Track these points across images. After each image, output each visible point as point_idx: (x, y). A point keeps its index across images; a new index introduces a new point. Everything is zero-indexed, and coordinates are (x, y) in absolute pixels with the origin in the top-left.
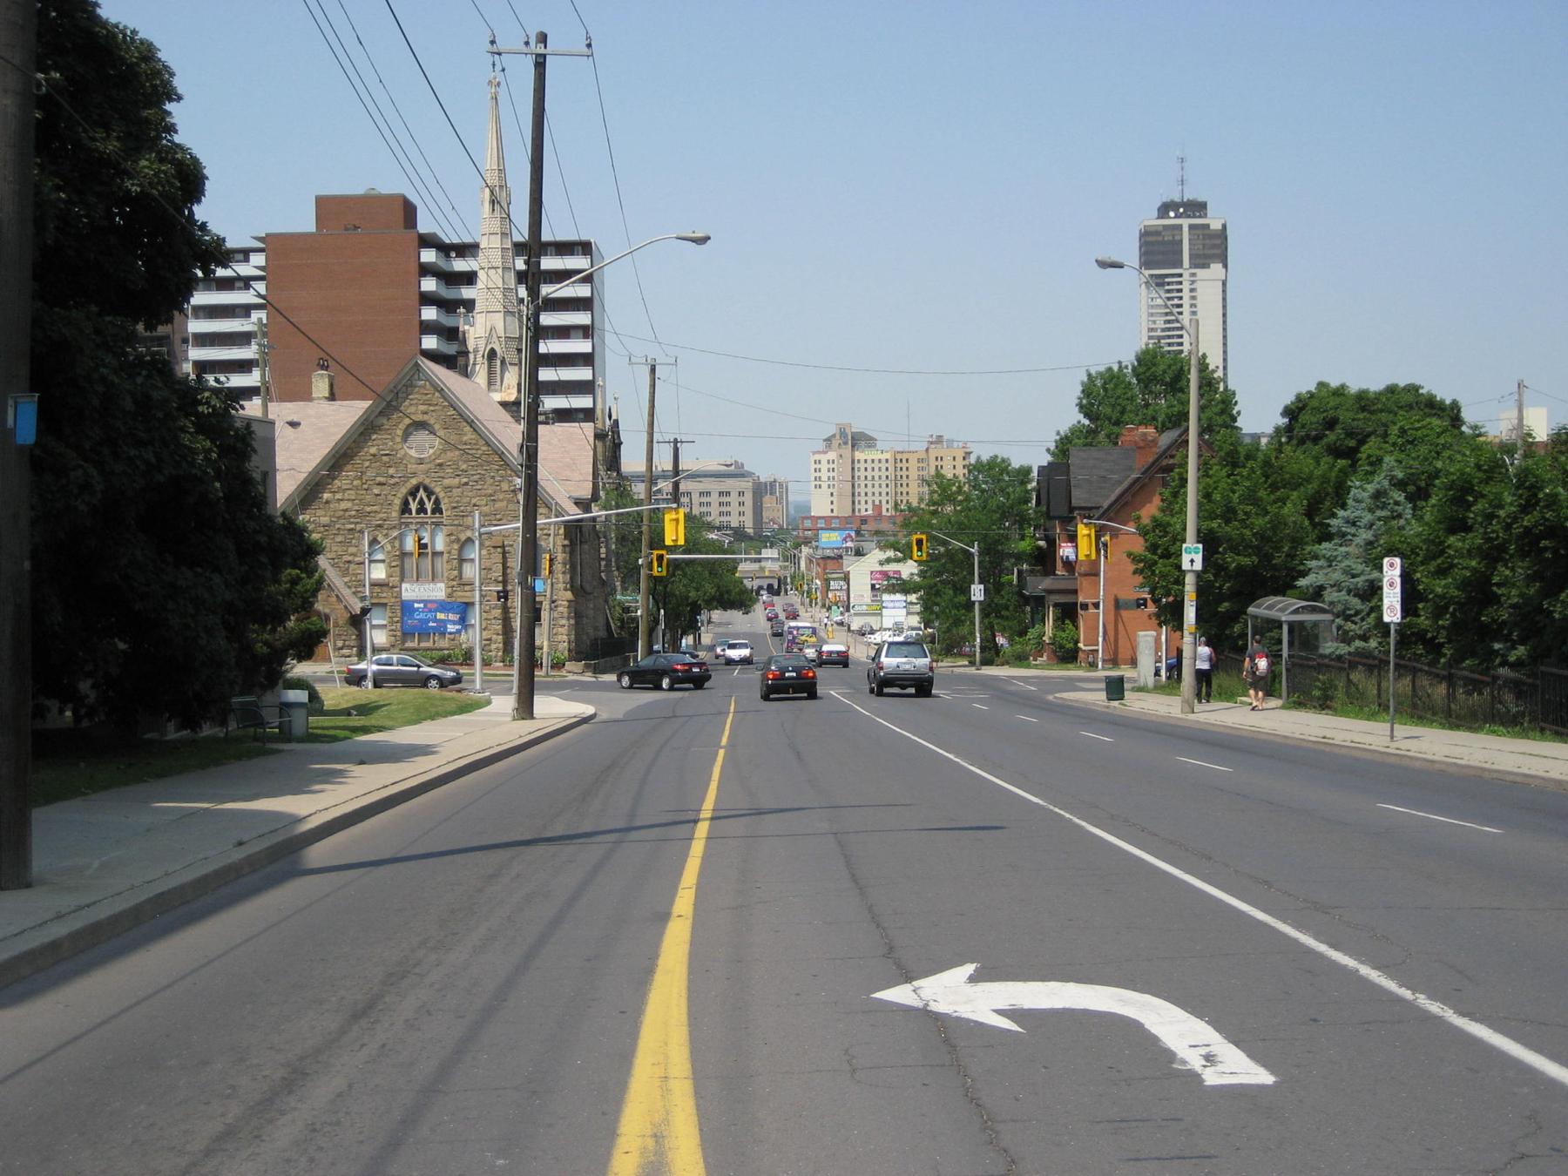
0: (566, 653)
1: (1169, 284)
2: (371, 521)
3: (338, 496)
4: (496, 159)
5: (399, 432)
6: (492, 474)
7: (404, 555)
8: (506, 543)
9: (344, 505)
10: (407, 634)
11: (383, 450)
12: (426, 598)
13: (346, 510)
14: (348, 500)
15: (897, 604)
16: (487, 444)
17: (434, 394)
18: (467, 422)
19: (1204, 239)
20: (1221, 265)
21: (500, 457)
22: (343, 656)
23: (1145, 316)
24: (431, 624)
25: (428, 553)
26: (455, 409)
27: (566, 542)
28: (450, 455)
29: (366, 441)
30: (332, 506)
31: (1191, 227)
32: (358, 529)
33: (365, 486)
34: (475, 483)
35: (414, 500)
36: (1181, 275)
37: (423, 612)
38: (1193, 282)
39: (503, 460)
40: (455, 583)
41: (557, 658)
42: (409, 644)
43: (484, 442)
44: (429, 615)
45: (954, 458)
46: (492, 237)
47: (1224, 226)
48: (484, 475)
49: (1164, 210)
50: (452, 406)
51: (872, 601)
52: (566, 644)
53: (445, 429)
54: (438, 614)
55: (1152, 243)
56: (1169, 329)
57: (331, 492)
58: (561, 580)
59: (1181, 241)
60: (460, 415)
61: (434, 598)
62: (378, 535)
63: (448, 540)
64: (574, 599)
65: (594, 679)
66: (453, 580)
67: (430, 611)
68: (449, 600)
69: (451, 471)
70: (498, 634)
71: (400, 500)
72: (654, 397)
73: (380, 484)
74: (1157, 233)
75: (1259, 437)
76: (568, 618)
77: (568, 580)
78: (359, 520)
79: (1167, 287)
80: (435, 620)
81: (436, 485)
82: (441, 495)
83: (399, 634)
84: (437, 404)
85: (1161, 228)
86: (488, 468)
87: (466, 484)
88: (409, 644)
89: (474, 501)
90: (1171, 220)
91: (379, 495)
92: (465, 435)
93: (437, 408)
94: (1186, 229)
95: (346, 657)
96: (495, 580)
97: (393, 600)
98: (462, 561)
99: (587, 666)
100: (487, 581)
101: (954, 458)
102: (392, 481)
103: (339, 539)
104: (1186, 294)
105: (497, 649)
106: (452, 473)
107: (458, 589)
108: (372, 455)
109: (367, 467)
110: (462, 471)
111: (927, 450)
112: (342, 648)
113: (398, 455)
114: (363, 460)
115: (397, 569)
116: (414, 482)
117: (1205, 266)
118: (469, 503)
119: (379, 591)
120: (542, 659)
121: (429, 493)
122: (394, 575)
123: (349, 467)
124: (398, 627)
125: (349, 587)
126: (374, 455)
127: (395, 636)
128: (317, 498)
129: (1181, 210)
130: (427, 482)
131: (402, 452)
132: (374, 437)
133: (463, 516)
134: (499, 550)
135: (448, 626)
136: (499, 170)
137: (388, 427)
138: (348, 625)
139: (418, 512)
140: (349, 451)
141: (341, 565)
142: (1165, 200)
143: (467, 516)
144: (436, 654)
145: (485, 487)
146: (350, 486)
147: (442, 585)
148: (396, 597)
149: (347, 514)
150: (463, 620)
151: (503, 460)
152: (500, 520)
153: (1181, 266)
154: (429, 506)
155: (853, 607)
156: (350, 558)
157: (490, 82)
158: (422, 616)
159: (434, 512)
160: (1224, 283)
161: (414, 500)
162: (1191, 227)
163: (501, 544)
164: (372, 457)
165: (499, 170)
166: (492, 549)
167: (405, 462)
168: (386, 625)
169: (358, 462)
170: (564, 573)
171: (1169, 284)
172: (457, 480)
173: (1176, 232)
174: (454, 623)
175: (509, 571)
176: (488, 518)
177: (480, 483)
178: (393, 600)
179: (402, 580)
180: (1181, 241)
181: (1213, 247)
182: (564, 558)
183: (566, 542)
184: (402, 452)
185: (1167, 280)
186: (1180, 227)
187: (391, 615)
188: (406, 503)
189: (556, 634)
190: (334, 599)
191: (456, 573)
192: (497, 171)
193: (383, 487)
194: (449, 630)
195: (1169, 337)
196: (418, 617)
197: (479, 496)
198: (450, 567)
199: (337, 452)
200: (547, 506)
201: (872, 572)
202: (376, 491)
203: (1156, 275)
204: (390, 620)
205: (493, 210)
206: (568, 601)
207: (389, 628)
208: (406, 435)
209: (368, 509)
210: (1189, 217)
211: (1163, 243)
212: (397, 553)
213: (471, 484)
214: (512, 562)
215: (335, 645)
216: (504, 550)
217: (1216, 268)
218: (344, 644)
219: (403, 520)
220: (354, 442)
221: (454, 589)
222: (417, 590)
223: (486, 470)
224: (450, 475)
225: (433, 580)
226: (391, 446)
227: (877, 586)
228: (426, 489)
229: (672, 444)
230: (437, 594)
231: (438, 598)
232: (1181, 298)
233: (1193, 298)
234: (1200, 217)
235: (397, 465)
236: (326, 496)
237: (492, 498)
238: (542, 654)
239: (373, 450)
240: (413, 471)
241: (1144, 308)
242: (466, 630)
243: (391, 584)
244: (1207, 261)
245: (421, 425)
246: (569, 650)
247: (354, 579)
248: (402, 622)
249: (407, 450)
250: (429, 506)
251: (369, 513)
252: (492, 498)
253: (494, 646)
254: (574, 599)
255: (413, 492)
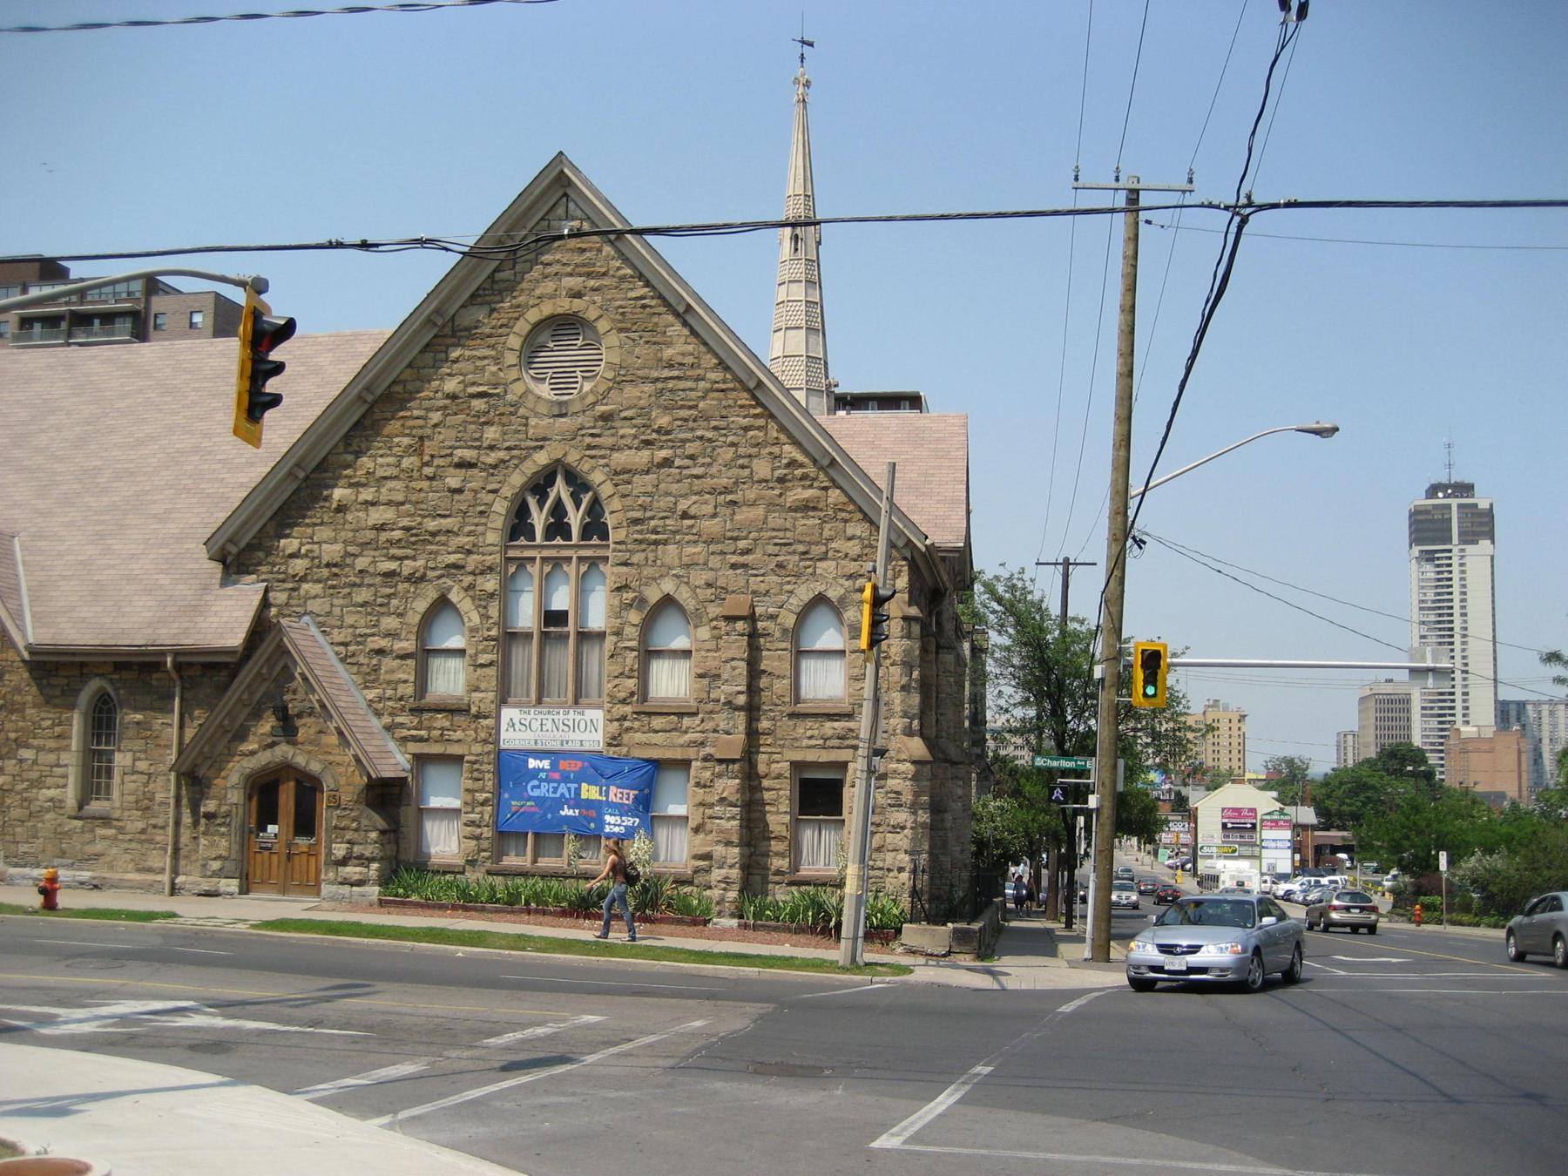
0: (905, 902)
1: (1438, 559)
2: (437, 553)
3: (367, 494)
4: (802, 180)
5: (514, 342)
6: (731, 439)
7: (510, 638)
8: (758, 610)
9: (377, 516)
10: (505, 837)
11: (474, 384)
12: (557, 747)
13: (381, 528)
14: (389, 503)
15: (1279, 844)
16: (722, 365)
17: (599, 250)
18: (677, 315)
19: (1472, 517)
20: (1489, 542)
21: (754, 397)
22: (345, 882)
23: (1415, 589)
24: (567, 812)
25: (567, 636)
26: (648, 284)
27: (914, 611)
28: (630, 392)
29: (436, 366)
30: (349, 517)
31: (1460, 506)
32: (406, 571)
33: (428, 471)
34: (687, 462)
35: (541, 504)
36: (1450, 551)
37: (548, 780)
38: (1462, 557)
39: (759, 404)
40: (628, 709)
41: (882, 911)
42: (511, 861)
43: (715, 361)
44: (563, 789)
45: (1230, 721)
46: (794, 286)
47: (1491, 505)
48: (710, 440)
49: (1433, 491)
50: (641, 276)
51: (1223, 842)
52: (905, 876)
53: (621, 330)
54: (584, 786)
55: (1421, 521)
56: (1439, 601)
57: (351, 485)
58: (897, 707)
59: (1451, 519)
60: (661, 297)
61: (577, 747)
62: (449, 589)
63: (617, 602)
64: (929, 757)
65: (983, 982)
66: (624, 701)
67: (566, 779)
68: (612, 752)
69: (633, 431)
70: (728, 843)
71: (506, 504)
72: (1135, 266)
73: (464, 465)
74: (1427, 512)
75: (1524, 705)
76: (914, 808)
77: (916, 711)
78: (409, 552)
79: (1437, 562)
80: (577, 802)
81: (593, 469)
82: (606, 490)
83: (487, 832)
84: (604, 274)
85: (1431, 508)
86: (723, 423)
87: (667, 463)
88: (511, 861)
89: (683, 505)
90: (1441, 499)
91: (459, 491)
92: (669, 344)
93: (606, 281)
94: (1454, 509)
95: (352, 885)
96: (729, 703)
97: (477, 748)
98: (648, 654)
99: (961, 937)
100: (710, 706)
101: (1230, 721)
102: (491, 459)
103: (363, 595)
104: (1455, 568)
105: (726, 881)
106: (635, 437)
107: (636, 724)
108: (448, 396)
109: (436, 426)
110: (658, 431)
111: (1204, 713)
112: (344, 862)
113: (509, 397)
114: (428, 410)
115: (492, 671)
116: (542, 458)
117: (1475, 542)
118: (672, 511)
119: (447, 724)
120: (840, 914)
121: (578, 485)
122: (483, 686)
123: (393, 426)
124: (486, 817)
125: (378, 714)
126: (453, 397)
127: (478, 838)
128: (316, 498)
129: (1449, 491)
130: (572, 458)
131: (518, 388)
132: (455, 354)
133: (656, 543)
134: (740, 625)
135: (608, 818)
136: (805, 196)
137: (487, 331)
138: (362, 807)
139: (550, 533)
140: (398, 388)
141: (362, 660)
142: (1433, 482)
143: (665, 543)
144: (573, 888)
145: (714, 470)
146: (395, 472)
147: (597, 715)
148: (485, 741)
149: (384, 536)
150: (645, 804)
151: (759, 404)
152: (748, 552)
153: (1451, 543)
154: (575, 519)
155: (1202, 848)
156: (383, 643)
157: (796, 82)
158: (544, 791)
159: (586, 532)
160: (1492, 558)
161: (541, 504)
162: (1460, 506)
163: (745, 613)
164: (448, 402)
165: (805, 196)
166: (723, 624)
167: (522, 411)
168: (457, 811)
169: (416, 413)
170: (905, 688)
171: (1438, 559)
172: (645, 454)
173: (1445, 511)
174: (621, 810)
175: (764, 682)
176: (719, 547)
177: (701, 460)
178: (477, 748)
179: (503, 699)
180: (1450, 520)
181: (1481, 525)
182: (908, 652)
183: (914, 611)
184: (518, 388)
185: (1437, 555)
186: (1449, 507)
187: (470, 784)
188: (520, 514)
189: (879, 849)
190: (333, 739)
191: (631, 684)
192: (802, 197)
193: (472, 472)
194: (607, 829)
195: (1439, 608)
196: (536, 793)
197: (699, 493)
198: (617, 669)
199: (368, 389)
200: (866, 518)
201: (1223, 809)
202: (453, 482)
203: (1426, 551)
204: (469, 798)
205: (796, 250)
206: (914, 762)
207: (465, 818)
208: (531, 350)
209: (432, 525)
210: (1457, 497)
211: (1432, 521)
212: (494, 633)
213: (678, 462)
214: (769, 658)
215: (329, 853)
216: (755, 629)
217: (1485, 544)
218: (350, 851)
219: (511, 553)
220: (410, 366)
221: (627, 724)
222: (536, 725)
223: (716, 428)
224: (628, 441)
225: (576, 702)
226: (493, 374)
227: (1229, 826)
228: (572, 478)
229: (1060, 568)
230: (585, 736)
231: (587, 747)
232: (1451, 572)
233: (1463, 572)
234: (1467, 497)
235: (504, 419)
236: (339, 493)
237: (729, 497)
238: (841, 899)
239: (451, 385)
240: (540, 433)
241: (1415, 582)
242: (651, 835)
243: (474, 710)
244: (1476, 538)
245: (566, 325)
246: (914, 893)
247: (389, 693)
248: (498, 803)
249: (532, 385)
250: (575, 519)
251: (433, 534)
252: (729, 497)
253: (717, 874)
254: (929, 757)
255: (540, 485)
